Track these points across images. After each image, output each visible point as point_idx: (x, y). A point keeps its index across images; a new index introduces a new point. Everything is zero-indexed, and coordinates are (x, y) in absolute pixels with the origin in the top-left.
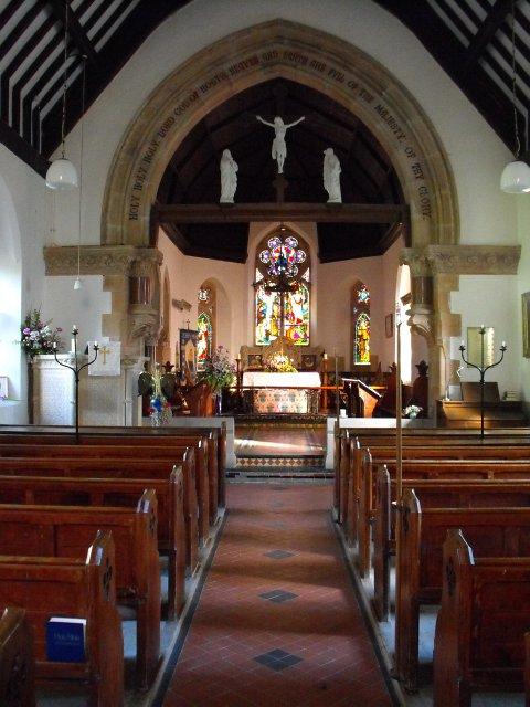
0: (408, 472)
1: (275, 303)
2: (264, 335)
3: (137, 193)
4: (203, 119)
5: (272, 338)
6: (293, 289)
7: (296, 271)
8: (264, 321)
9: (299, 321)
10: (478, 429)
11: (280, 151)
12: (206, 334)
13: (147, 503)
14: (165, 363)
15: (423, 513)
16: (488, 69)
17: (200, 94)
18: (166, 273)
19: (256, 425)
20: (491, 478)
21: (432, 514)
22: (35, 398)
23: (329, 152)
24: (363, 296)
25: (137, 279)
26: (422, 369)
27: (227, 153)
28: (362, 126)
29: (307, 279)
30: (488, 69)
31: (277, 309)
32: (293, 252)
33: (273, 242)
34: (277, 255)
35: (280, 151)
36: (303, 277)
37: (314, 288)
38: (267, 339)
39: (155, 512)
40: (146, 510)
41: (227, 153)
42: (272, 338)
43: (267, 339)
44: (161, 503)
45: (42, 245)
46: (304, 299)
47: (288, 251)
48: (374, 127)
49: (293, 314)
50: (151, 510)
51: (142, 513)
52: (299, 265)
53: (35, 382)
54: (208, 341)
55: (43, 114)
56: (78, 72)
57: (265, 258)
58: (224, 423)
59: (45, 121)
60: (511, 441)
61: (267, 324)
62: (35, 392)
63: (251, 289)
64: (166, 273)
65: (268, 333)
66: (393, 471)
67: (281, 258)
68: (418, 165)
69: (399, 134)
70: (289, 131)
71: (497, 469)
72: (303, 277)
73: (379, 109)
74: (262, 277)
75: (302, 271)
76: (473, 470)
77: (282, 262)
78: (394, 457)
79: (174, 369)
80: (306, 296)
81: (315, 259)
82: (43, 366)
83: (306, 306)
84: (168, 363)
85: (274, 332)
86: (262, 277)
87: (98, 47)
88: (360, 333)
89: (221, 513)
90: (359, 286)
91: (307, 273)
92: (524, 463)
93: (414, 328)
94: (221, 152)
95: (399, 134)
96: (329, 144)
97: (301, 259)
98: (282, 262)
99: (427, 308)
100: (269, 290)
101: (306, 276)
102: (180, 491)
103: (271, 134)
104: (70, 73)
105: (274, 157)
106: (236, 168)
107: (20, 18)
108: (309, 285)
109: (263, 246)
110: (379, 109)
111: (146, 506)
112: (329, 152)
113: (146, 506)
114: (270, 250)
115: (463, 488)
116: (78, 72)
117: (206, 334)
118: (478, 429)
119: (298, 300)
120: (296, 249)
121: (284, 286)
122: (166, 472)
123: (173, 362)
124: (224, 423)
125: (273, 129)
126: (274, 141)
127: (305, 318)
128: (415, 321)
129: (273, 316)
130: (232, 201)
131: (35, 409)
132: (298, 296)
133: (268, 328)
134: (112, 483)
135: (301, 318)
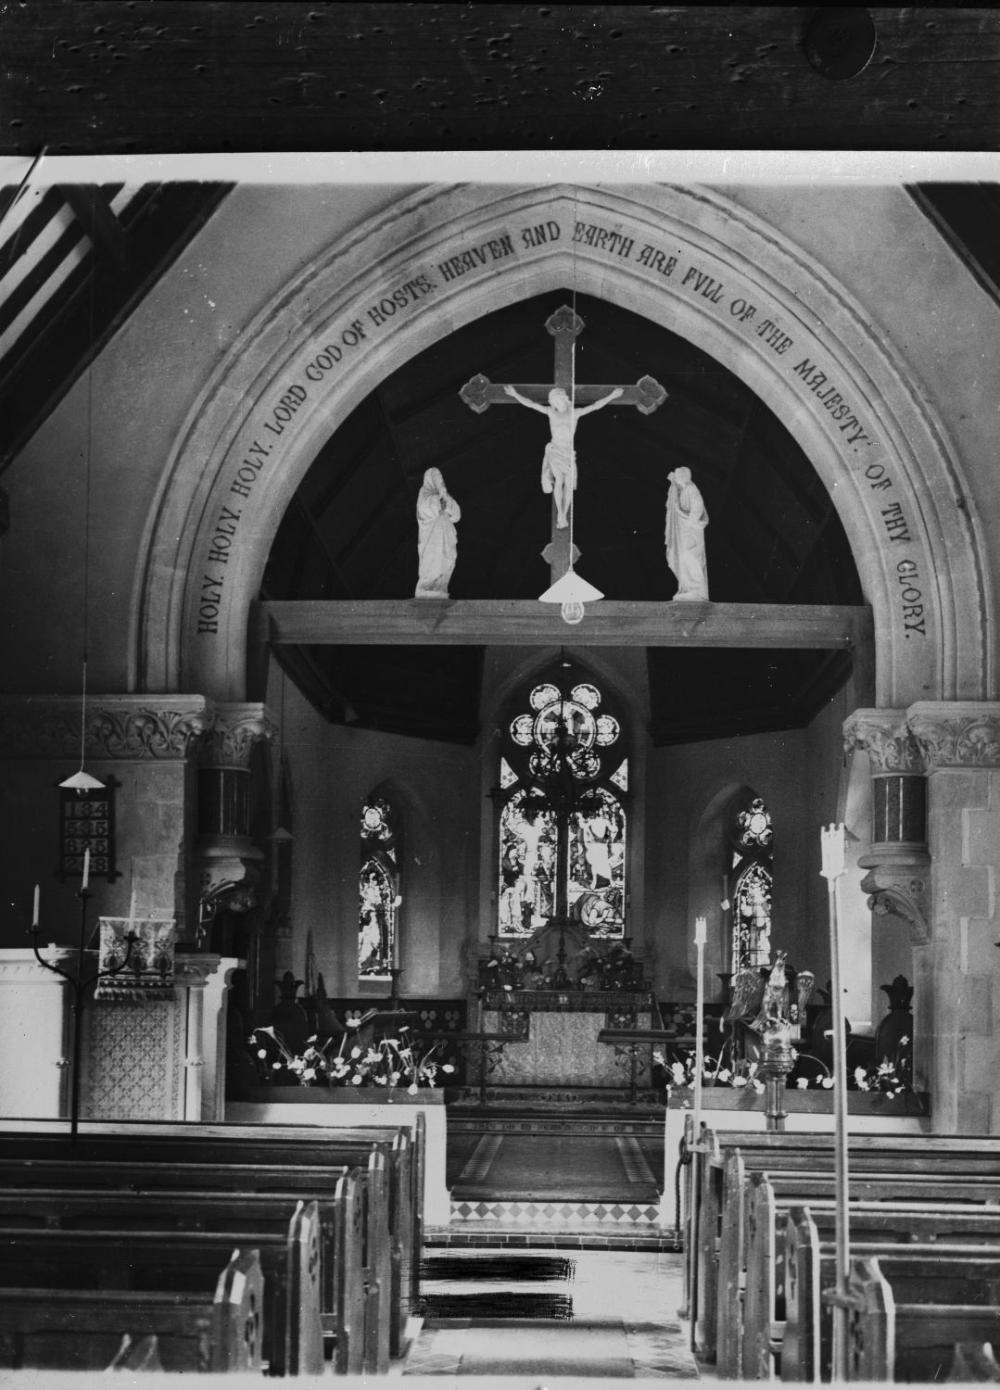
1: (545, 839)
2: (518, 911)
3: (679, 272)
6: (591, 808)
8: (520, 883)
11: (560, 470)
17: (369, 328)
18: (285, 761)
21: (920, 1316)
23: (681, 477)
26: (896, 993)
27: (433, 477)
29: (624, 785)
31: (549, 854)
32: (589, 720)
34: (552, 726)
35: (560, 470)
36: (614, 778)
38: (526, 923)
39: (259, 1302)
40: (236, 1298)
41: (433, 477)
42: (538, 922)
43: (526, 923)
47: (577, 717)
50: (251, 1299)
51: (226, 1307)
54: (384, 932)
56: (71, 262)
61: (526, 888)
63: (487, 805)
64: (285, 761)
65: (528, 911)
66: (827, 1230)
67: (561, 731)
68: (897, 507)
69: (851, 432)
72: (614, 778)
74: (515, 778)
75: (609, 767)
77: (564, 743)
78: (831, 1197)
80: (620, 824)
83: (619, 848)
84: (289, 975)
85: (541, 907)
86: (515, 778)
88: (748, 911)
91: (623, 769)
92: (998, 1178)
93: (877, 897)
95: (851, 432)
97: (607, 738)
100: (530, 809)
101: (621, 777)
103: (540, 430)
105: (547, 488)
106: (454, 512)
110: (804, 368)
112: (681, 477)
116: (71, 262)
117: (381, 913)
119: (601, 835)
124: (421, 1119)
125: (545, 418)
126: (548, 448)
127: (615, 876)
129: (540, 871)
130: (445, 595)
132: (599, 824)
133: (529, 898)
134: (73, 1166)
135: (608, 875)
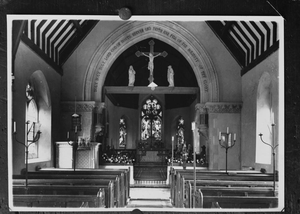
0: (198, 185)
1: (149, 124)
5: (148, 137)
6: (156, 119)
7: (156, 112)
9: (158, 131)
10: (271, 186)
11: (151, 66)
12: (123, 135)
16: (232, 33)
20: (229, 187)
23: (170, 67)
25: (97, 114)
26: (203, 148)
27: (131, 67)
29: (161, 115)
30: (232, 33)
32: (155, 105)
35: (151, 66)
36: (159, 114)
38: (146, 137)
41: (131, 67)
43: (146, 137)
44: (106, 194)
45: (188, 46)
46: (159, 122)
48: (187, 57)
49: (155, 128)
51: (99, 197)
55: (59, 49)
56: (73, 32)
61: (146, 132)
63: (140, 119)
65: (146, 135)
66: (192, 185)
67: (151, 107)
69: (196, 60)
72: (159, 114)
74: (144, 114)
77: (152, 109)
78: (193, 180)
79: (110, 148)
80: (160, 122)
82: (60, 146)
83: (160, 125)
84: (109, 146)
86: (144, 114)
88: (180, 135)
89: (128, 200)
91: (161, 113)
96: (15, 121)
98: (152, 109)
99: (205, 126)
100: (146, 119)
101: (161, 114)
102: (112, 190)
107: (49, 34)
112: (170, 67)
114: (147, 104)
116: (73, 32)
118: (271, 186)
123: (110, 145)
125: (149, 58)
128: (201, 131)
129: (148, 129)
130: (133, 86)
131: (62, 183)
132: (157, 122)
133: (146, 133)
135: (158, 130)
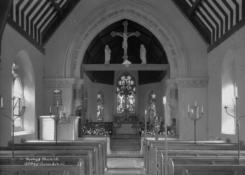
0: (169, 154)
4: (99, 34)
6: (130, 94)
13: (81, 163)
14: (86, 119)
15: (174, 166)
16: (198, 14)
19: (117, 140)
20: (198, 156)
22: (40, 131)
23: (142, 46)
24: (154, 96)
27: (107, 46)
28: (153, 36)
30: (198, 14)
32: (130, 81)
33: (123, 78)
36: (133, 90)
37: (137, 94)
40: (80, 166)
41: (107, 46)
43: (121, 111)
50: (82, 165)
51: (79, 167)
52: (131, 85)
53: (40, 124)
54: (101, 112)
55: (42, 30)
56: (54, 15)
57: (120, 83)
58: (106, 139)
59: (42, 33)
60: (177, 145)
62: (40, 126)
65: (121, 109)
67: (126, 83)
69: (166, 39)
70: (128, 38)
71: (200, 153)
72: (133, 90)
73: (160, 30)
74: (119, 90)
75: (133, 88)
76: (209, 155)
77: (126, 85)
81: (137, 83)
83: (134, 100)
84: (87, 119)
86: (119, 90)
87: (61, 6)
88: (153, 109)
89: (106, 169)
90: (152, 93)
91: (135, 89)
92: (244, 151)
94: (105, 45)
95: (166, 39)
100: (121, 94)
101: (134, 89)
103: (122, 39)
104: (51, 15)
106: (110, 51)
108: (135, 93)
109: (120, 79)
111: (81, 164)
112: (142, 46)
113: (81, 164)
114: (122, 80)
115: (188, 159)
120: (131, 80)
121: (126, 93)
122: (86, 154)
126: (123, 42)
128: (172, 104)
132: (131, 97)
133: (121, 107)
135: (132, 104)
